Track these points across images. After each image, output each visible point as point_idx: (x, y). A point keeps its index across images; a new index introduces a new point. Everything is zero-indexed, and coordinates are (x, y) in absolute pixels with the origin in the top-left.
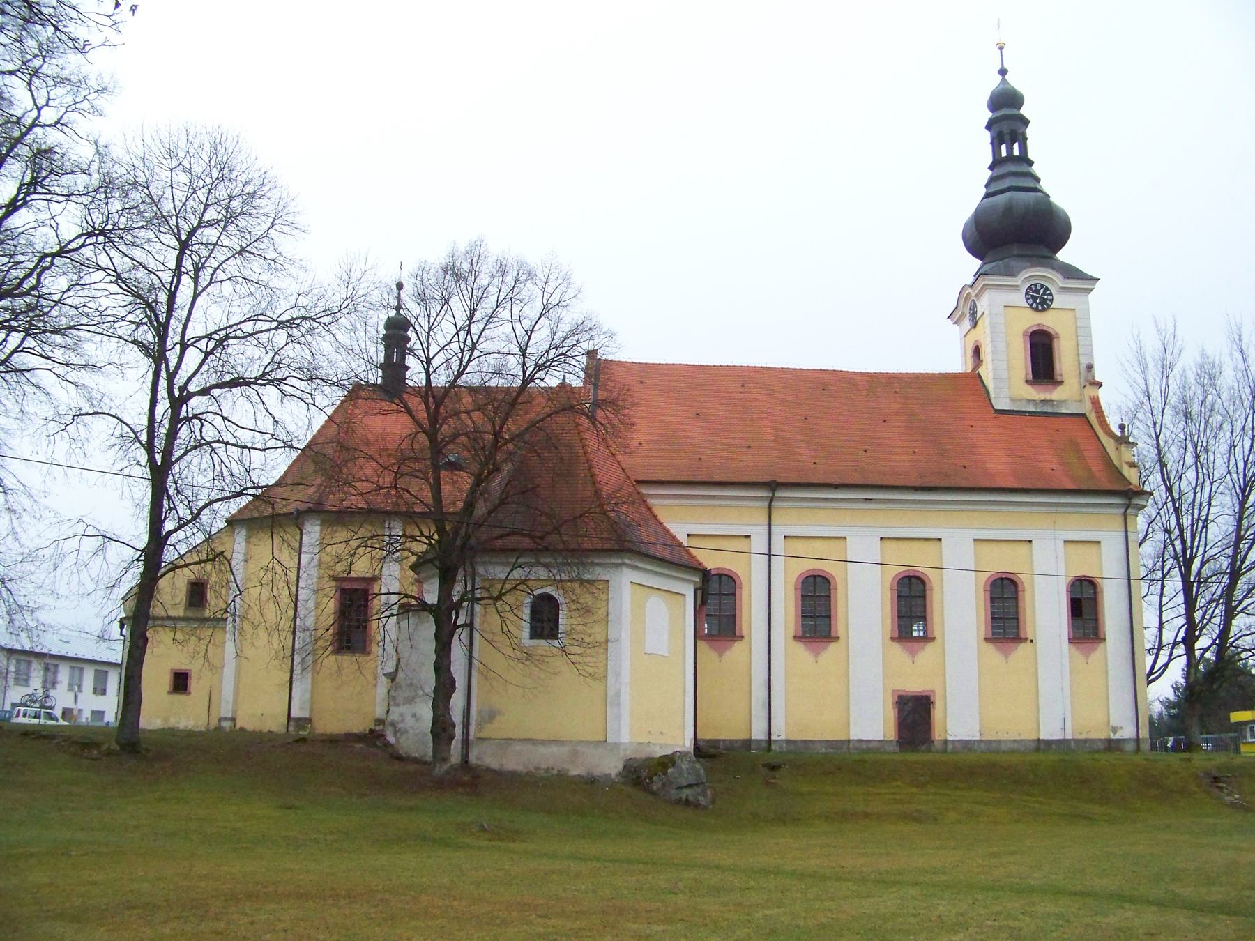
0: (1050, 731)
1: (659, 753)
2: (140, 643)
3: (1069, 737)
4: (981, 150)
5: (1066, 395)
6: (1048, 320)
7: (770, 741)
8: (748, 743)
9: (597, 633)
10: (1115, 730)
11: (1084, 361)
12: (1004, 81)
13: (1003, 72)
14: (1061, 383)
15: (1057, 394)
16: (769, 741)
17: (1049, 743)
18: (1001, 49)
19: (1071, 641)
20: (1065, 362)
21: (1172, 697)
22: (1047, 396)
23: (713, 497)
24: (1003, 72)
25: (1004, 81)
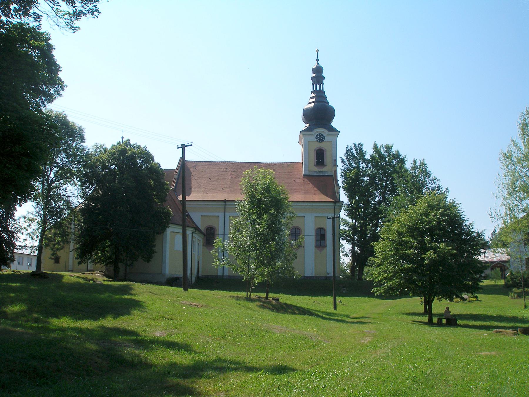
0: (308, 274)
1: (175, 276)
2: (263, 165)
3: (314, 275)
4: (309, 86)
5: (327, 170)
6: (322, 145)
7: (223, 276)
8: (217, 276)
9: (154, 244)
10: (328, 274)
11: (334, 158)
12: (318, 64)
13: (318, 60)
14: (326, 166)
15: (324, 169)
16: (223, 276)
17: (307, 277)
18: (318, 51)
19: (203, 245)
20: (328, 159)
21: (154, 248)
22: (321, 170)
23: (198, 204)
24: (318, 60)
25: (318, 64)
